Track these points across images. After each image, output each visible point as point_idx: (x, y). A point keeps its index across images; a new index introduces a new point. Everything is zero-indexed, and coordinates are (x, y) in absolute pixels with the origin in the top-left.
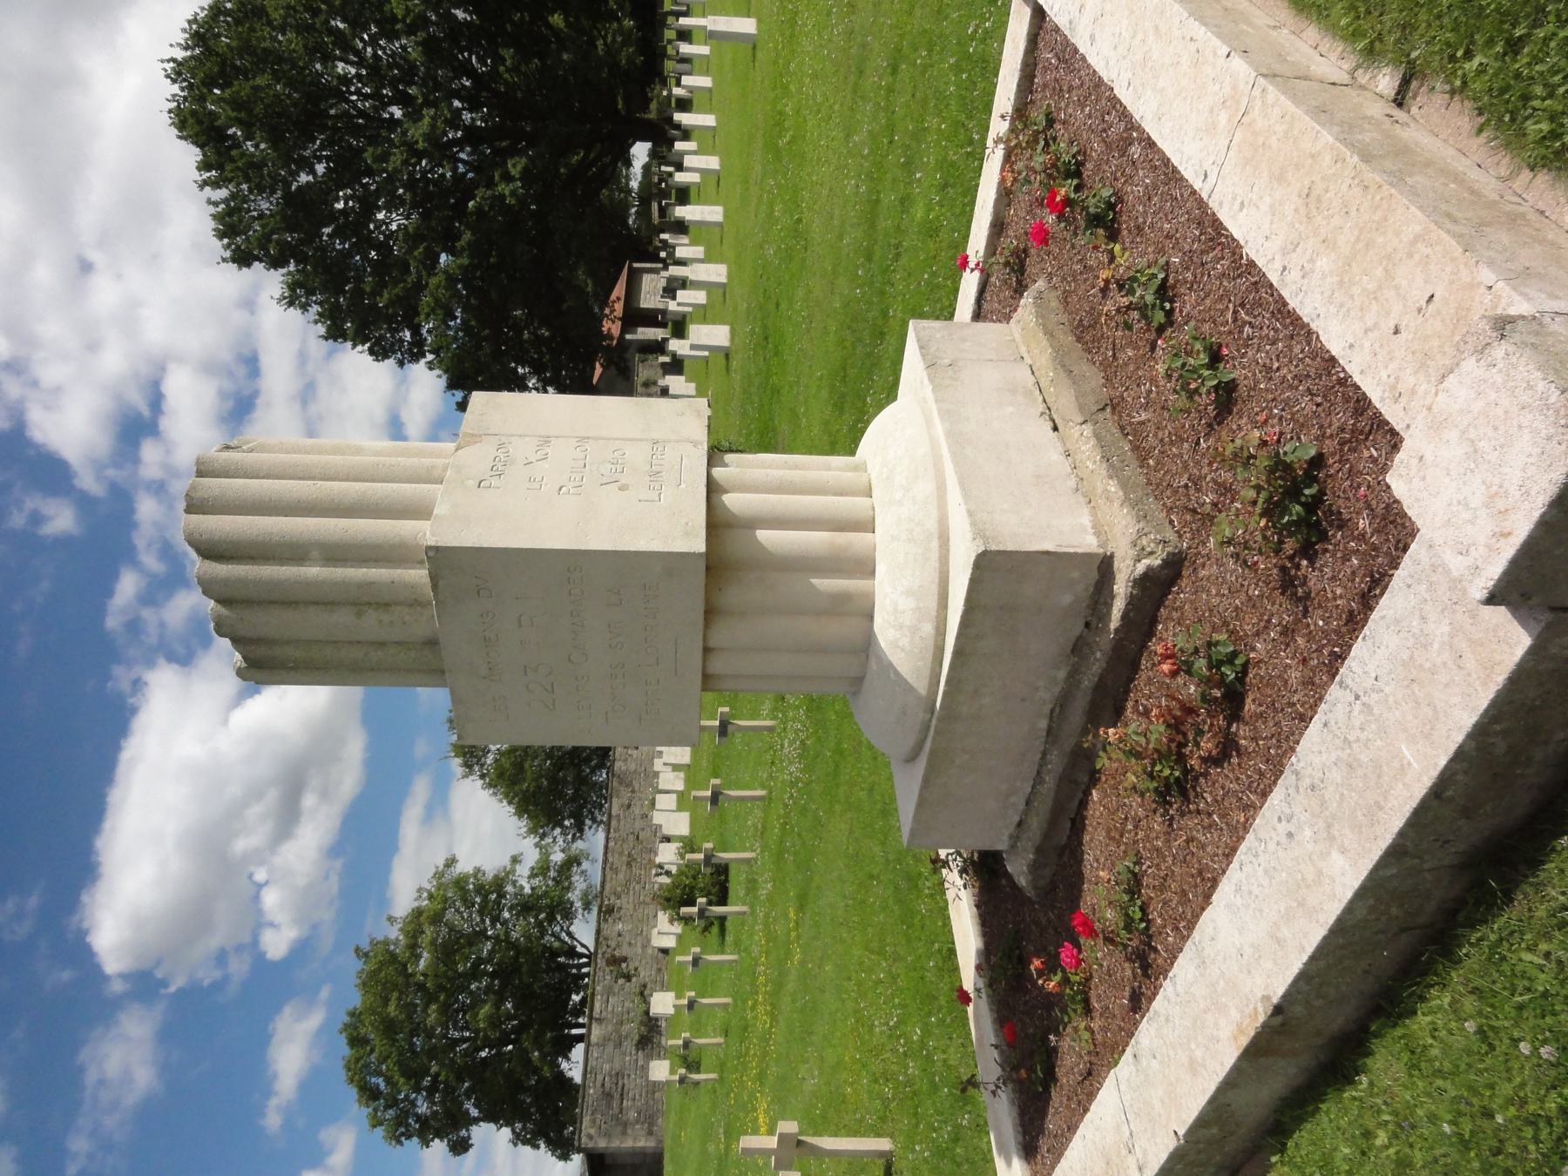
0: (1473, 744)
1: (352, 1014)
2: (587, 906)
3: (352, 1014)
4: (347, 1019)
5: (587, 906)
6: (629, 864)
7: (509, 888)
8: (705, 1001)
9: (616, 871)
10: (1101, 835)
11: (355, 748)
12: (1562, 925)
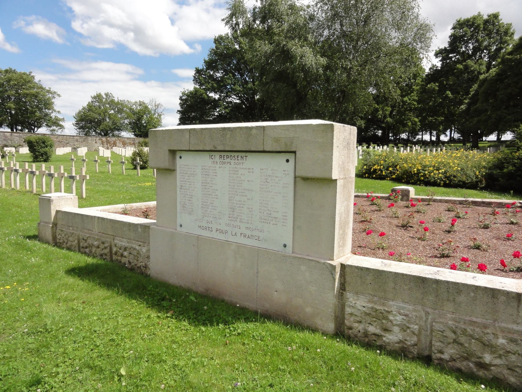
0: (454, 374)
1: (15, 70)
2: (51, 131)
3: (15, 70)
4: (13, 69)
5: (51, 131)
6: (59, 141)
7: (51, 111)
8: (14, 158)
9: (57, 138)
10: (435, 276)
11: (148, 52)
12: (435, 391)
